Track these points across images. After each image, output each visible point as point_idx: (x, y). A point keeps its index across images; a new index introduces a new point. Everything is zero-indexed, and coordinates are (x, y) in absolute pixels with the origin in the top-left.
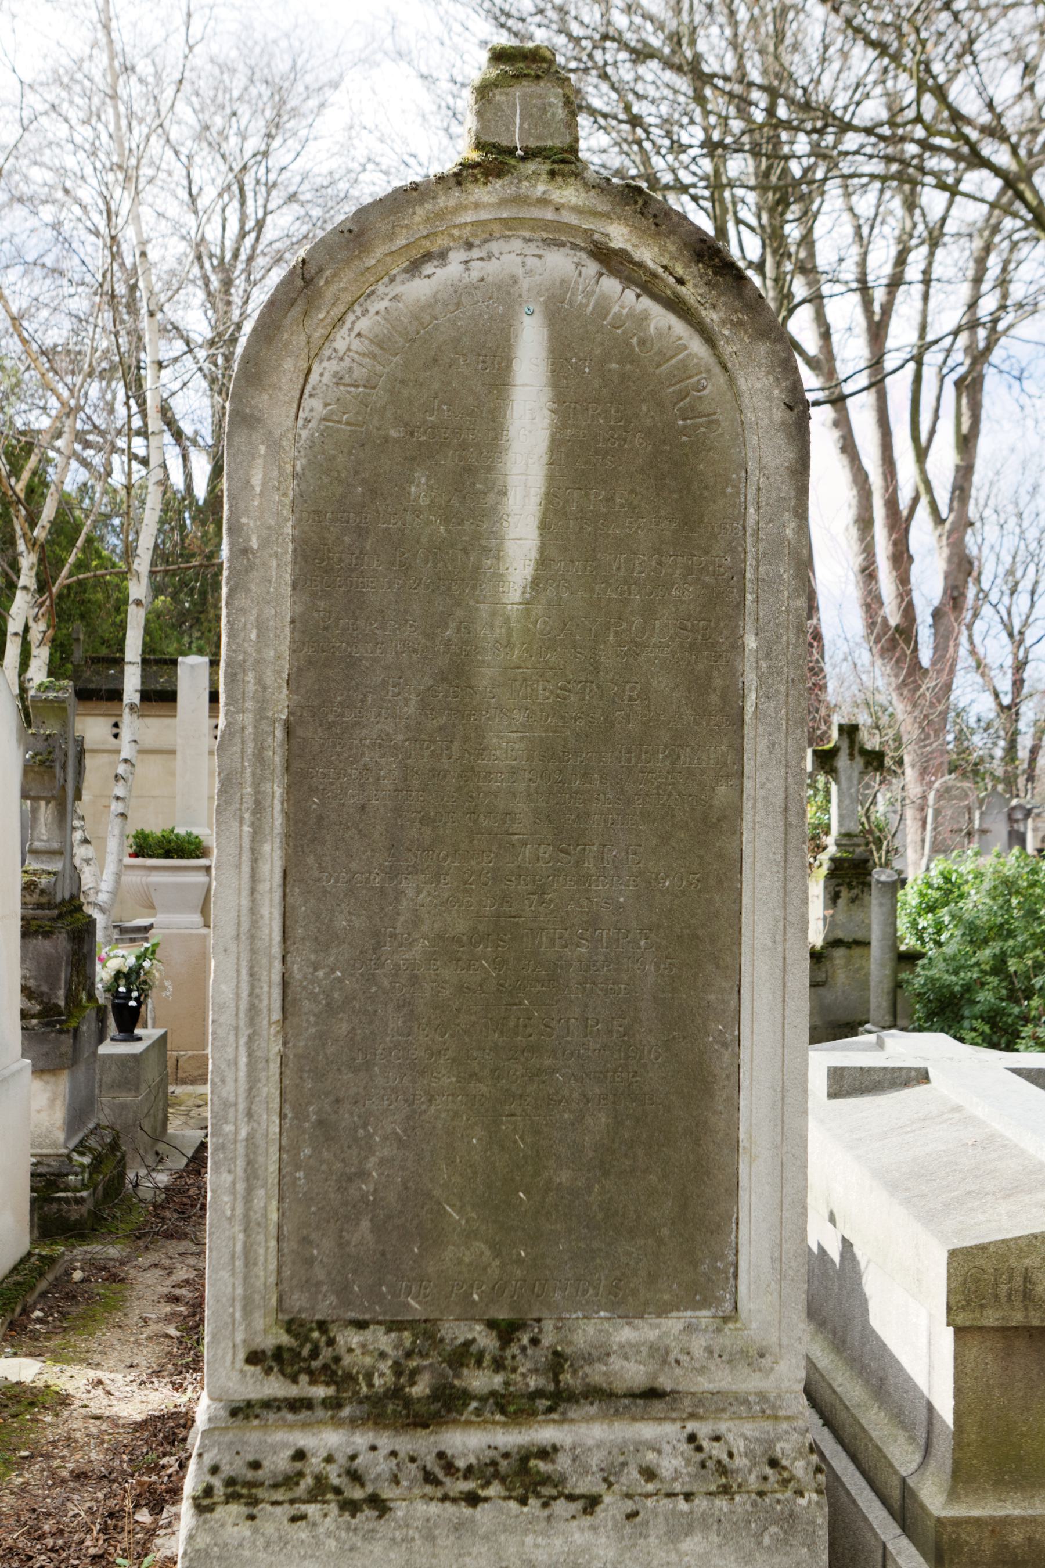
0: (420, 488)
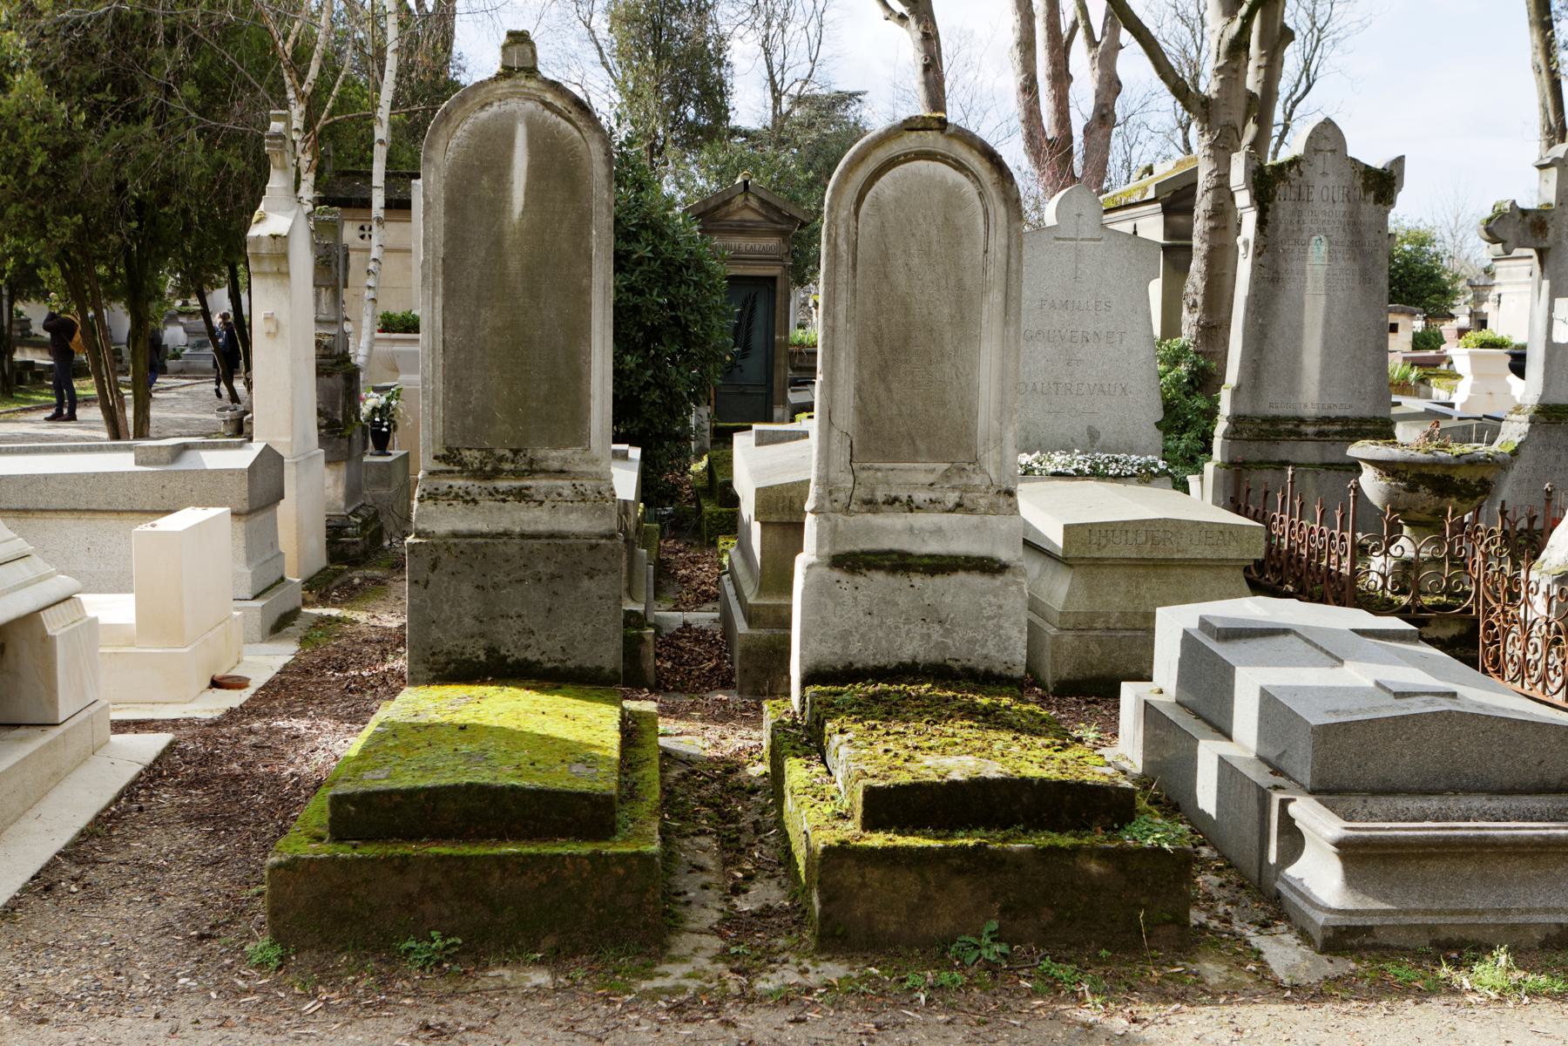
0: (485, 182)
